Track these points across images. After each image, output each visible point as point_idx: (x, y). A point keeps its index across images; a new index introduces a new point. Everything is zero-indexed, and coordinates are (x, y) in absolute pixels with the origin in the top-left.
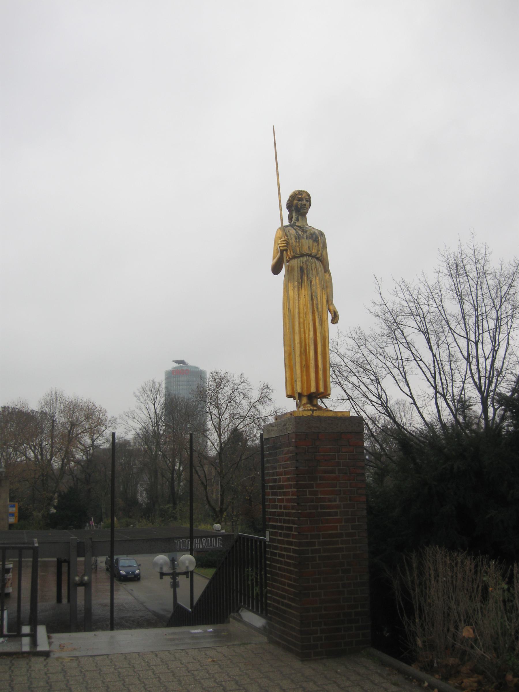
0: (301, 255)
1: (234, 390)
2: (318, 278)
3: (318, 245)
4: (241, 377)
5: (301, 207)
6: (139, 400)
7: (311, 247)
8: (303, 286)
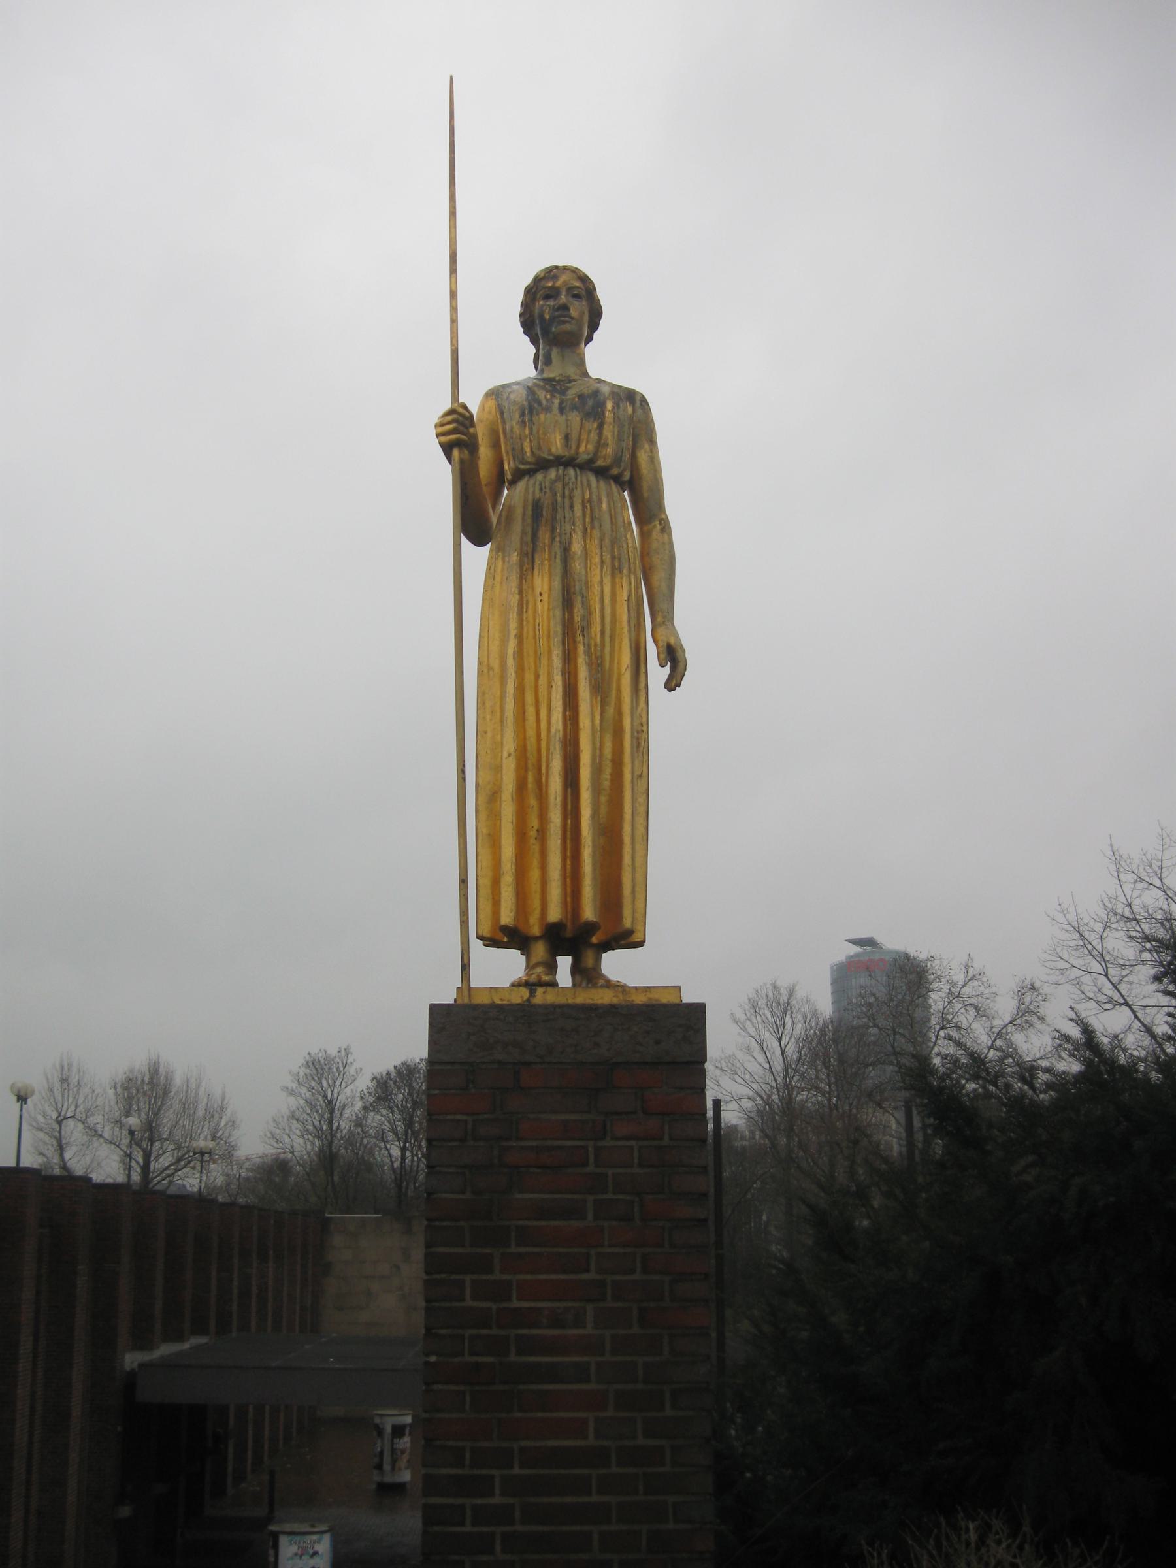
0: (556, 477)
1: (953, 997)
2: (596, 533)
3: (601, 427)
4: (967, 967)
5: (553, 319)
6: (744, 1029)
7: (574, 436)
8: (537, 562)
